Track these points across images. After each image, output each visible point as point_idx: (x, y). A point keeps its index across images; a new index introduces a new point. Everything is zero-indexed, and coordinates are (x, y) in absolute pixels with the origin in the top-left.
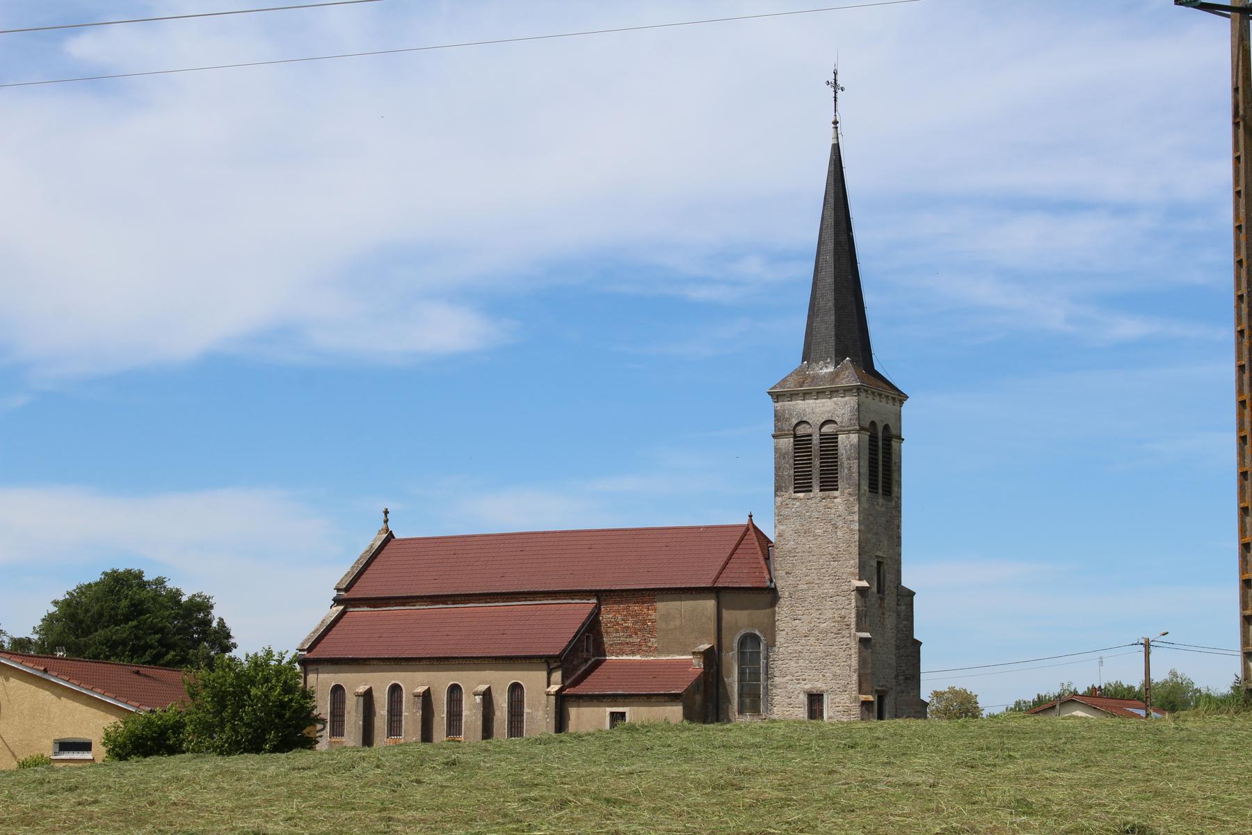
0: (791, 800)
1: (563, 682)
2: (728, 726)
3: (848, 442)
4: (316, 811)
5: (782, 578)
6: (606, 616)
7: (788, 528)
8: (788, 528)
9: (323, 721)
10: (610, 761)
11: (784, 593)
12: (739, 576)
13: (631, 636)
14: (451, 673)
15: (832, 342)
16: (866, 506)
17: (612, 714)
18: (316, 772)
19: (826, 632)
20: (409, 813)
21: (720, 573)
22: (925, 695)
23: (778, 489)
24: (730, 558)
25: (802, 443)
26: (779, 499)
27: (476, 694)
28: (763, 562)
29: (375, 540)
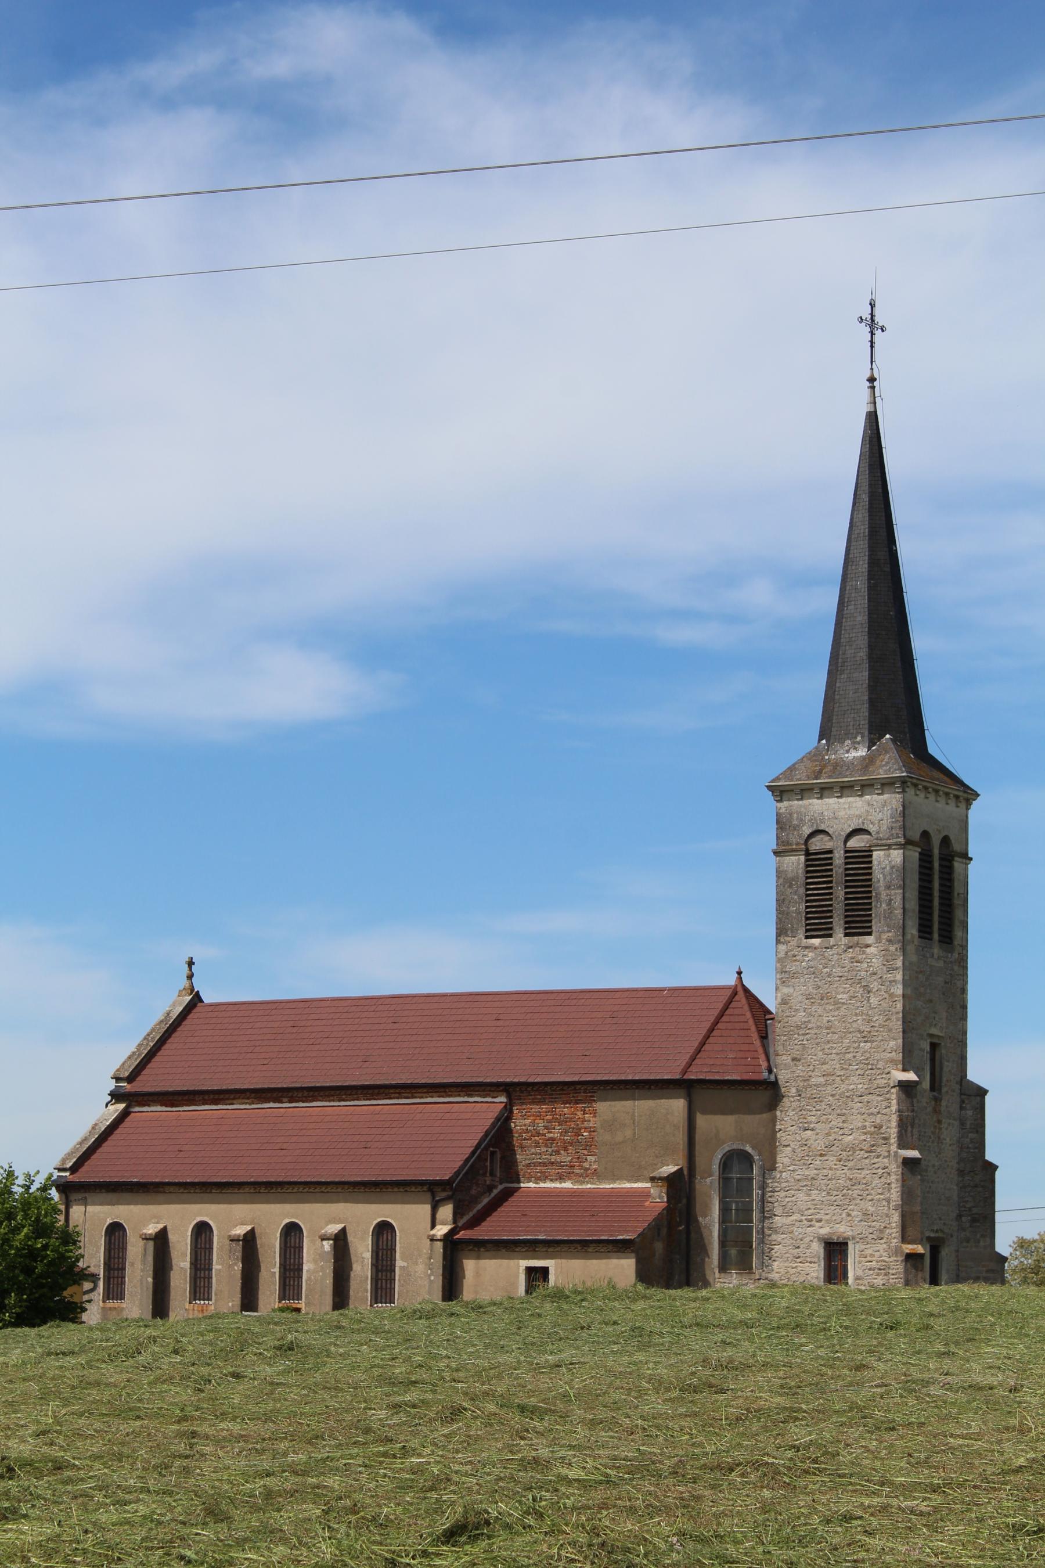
0: (799, 1410)
1: (455, 1221)
2: (704, 1293)
3: (887, 861)
4: (82, 1421)
5: (787, 1067)
6: (520, 1123)
7: (797, 992)
8: (797, 992)
9: (93, 1278)
10: (527, 1346)
11: (789, 1090)
12: (723, 1064)
13: (558, 1153)
15: (864, 710)
16: (914, 958)
17: (530, 1270)
18: (82, 1359)
20: (223, 1425)
21: (693, 1058)
22: (1003, 1244)
23: (781, 932)
24: (707, 1037)
25: (817, 864)
26: (783, 948)
27: (323, 1238)
28: (757, 1043)
29: (174, 1005)
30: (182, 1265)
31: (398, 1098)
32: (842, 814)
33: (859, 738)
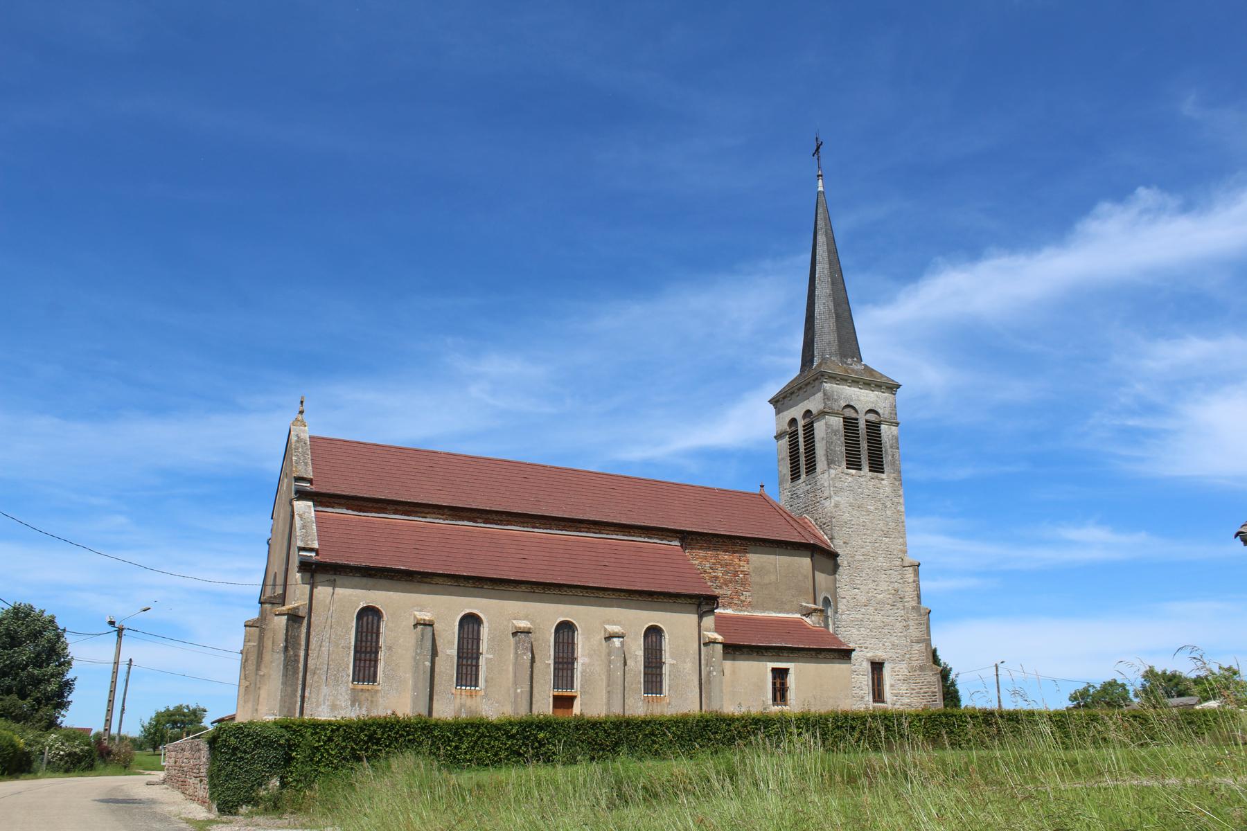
13: (721, 587)
14: (561, 607)
17: (774, 670)
19: (882, 602)
30: (448, 652)
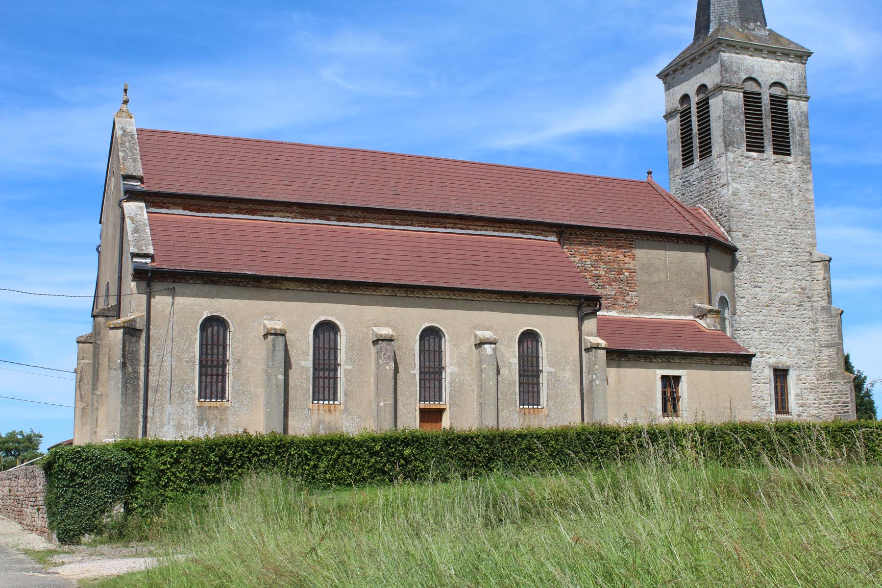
13: (603, 287)
17: (664, 378)
19: (787, 302)
30: (303, 364)
31: (452, 228)
32: (766, 69)
33: (759, 24)
